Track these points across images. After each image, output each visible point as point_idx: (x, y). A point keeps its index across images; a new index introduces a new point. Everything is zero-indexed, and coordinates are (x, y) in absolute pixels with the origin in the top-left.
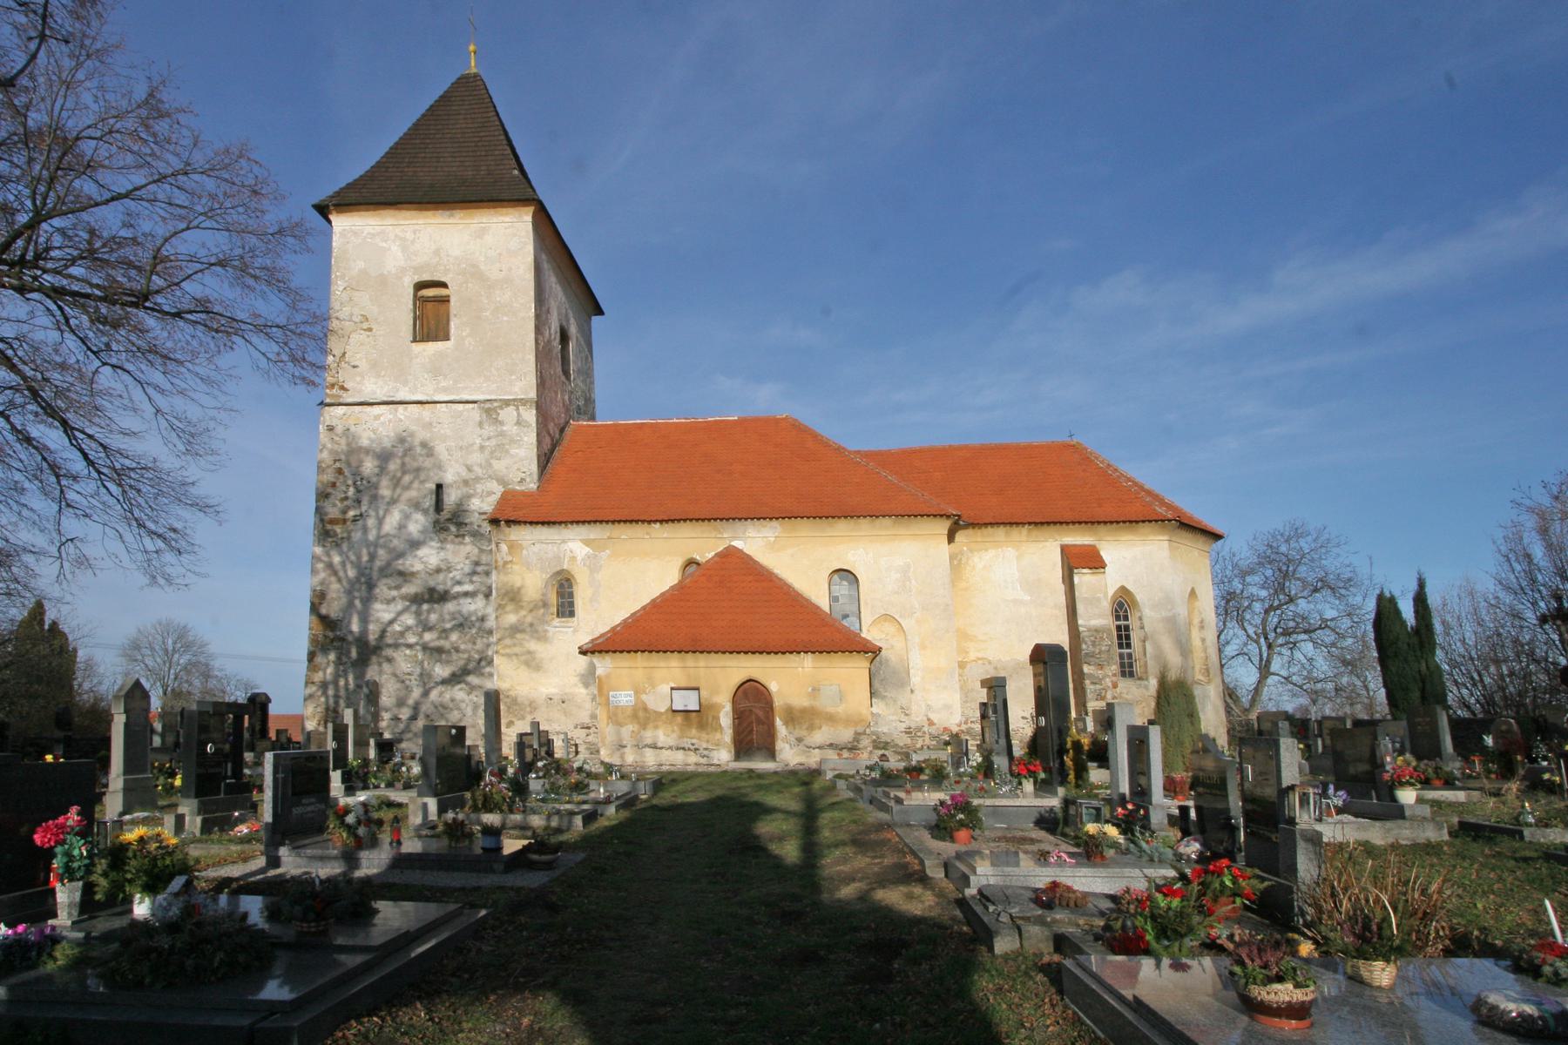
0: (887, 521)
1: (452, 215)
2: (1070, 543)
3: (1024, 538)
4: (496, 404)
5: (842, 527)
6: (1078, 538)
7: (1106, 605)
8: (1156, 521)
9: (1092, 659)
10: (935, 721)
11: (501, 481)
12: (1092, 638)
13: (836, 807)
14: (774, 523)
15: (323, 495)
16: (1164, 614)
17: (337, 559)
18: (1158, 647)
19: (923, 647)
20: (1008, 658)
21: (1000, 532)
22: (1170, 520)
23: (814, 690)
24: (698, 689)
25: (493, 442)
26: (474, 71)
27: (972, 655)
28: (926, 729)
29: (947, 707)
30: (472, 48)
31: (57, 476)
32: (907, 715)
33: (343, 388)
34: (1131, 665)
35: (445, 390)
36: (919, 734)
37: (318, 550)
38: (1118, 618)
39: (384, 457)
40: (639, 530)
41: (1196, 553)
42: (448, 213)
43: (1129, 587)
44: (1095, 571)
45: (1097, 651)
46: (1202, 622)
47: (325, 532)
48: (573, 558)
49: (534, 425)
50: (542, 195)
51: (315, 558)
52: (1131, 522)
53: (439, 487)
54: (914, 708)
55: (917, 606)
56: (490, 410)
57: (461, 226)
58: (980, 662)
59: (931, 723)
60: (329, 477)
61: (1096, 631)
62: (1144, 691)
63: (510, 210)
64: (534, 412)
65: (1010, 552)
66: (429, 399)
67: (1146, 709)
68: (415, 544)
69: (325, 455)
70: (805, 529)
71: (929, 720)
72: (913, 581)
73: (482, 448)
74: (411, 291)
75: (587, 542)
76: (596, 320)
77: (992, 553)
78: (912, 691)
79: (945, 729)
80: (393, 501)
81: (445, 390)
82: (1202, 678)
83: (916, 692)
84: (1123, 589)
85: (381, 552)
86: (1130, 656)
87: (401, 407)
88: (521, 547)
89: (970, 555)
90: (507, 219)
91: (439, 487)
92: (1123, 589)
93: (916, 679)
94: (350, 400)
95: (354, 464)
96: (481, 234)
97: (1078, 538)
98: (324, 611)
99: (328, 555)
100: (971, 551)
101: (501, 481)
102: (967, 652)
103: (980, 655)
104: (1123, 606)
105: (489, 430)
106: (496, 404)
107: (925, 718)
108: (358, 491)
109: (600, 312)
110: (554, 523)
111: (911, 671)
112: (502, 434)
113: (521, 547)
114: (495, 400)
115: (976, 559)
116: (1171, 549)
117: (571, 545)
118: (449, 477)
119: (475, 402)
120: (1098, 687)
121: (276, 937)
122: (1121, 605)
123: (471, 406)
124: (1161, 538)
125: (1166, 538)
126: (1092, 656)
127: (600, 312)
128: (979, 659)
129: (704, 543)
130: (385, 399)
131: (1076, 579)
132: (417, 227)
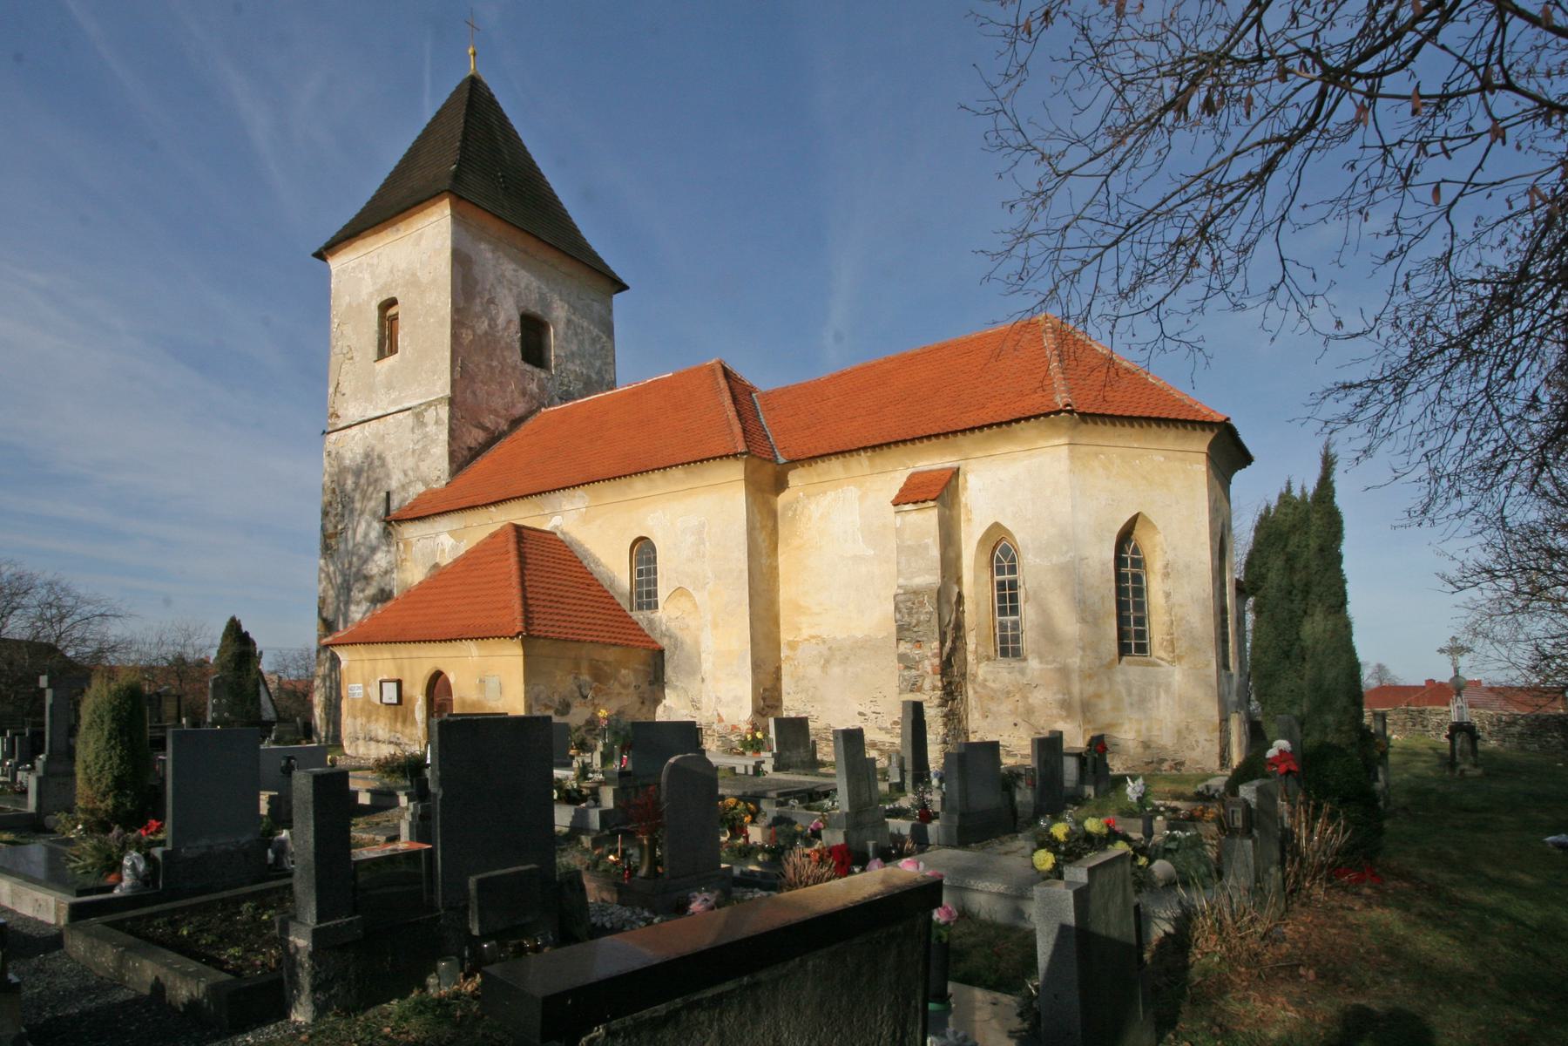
0: (677, 473)
1: (398, 230)
2: (926, 468)
3: (868, 471)
4: (423, 407)
5: (639, 485)
6: (932, 460)
8: (1047, 415)
9: (907, 633)
10: (724, 718)
11: (425, 483)
12: (909, 604)
14: (579, 492)
15: (325, 514)
16: (1055, 559)
17: (332, 569)
18: (1044, 611)
19: (715, 626)
20: (845, 636)
21: (835, 466)
22: (1057, 413)
23: (480, 681)
24: (381, 682)
25: (421, 444)
27: (806, 633)
28: (715, 726)
29: (737, 699)
32: (698, 709)
33: (338, 417)
34: (1016, 639)
35: (394, 402)
36: (709, 732)
37: (322, 562)
39: (358, 473)
41: (1158, 458)
42: (394, 229)
43: (1005, 524)
44: (921, 505)
45: (914, 622)
46: (1166, 566)
47: (327, 549)
49: (447, 421)
51: (321, 569)
52: (999, 424)
53: (388, 494)
54: (705, 700)
55: (710, 575)
56: (418, 413)
57: (406, 238)
58: (814, 641)
59: (721, 720)
60: (327, 498)
61: (915, 593)
62: (1019, 677)
63: (434, 209)
64: (447, 408)
65: (852, 492)
66: (385, 413)
67: (1020, 704)
68: (374, 550)
69: (326, 478)
70: (609, 492)
71: (719, 715)
72: (708, 544)
73: (414, 451)
74: (376, 313)
76: (618, 298)
77: (831, 495)
78: (703, 680)
79: (734, 727)
80: (362, 513)
81: (394, 402)
82: (1163, 654)
83: (707, 681)
85: (355, 559)
86: (1016, 625)
87: (366, 425)
89: (806, 502)
90: (434, 219)
91: (388, 494)
93: (707, 666)
94: (341, 426)
95: (342, 483)
96: (417, 242)
97: (948, 459)
98: (325, 615)
99: (327, 566)
100: (808, 497)
101: (425, 483)
102: (799, 629)
103: (813, 632)
105: (418, 434)
106: (423, 407)
107: (715, 713)
108: (344, 507)
109: (621, 287)
110: (428, 517)
111: (703, 656)
112: (425, 436)
114: (421, 404)
115: (813, 507)
116: (1072, 457)
118: (394, 484)
119: (409, 409)
120: (914, 672)
123: (407, 413)
124: (1056, 442)
125: (1064, 440)
126: (908, 630)
127: (621, 287)
128: (813, 637)
130: (360, 420)
132: (379, 251)
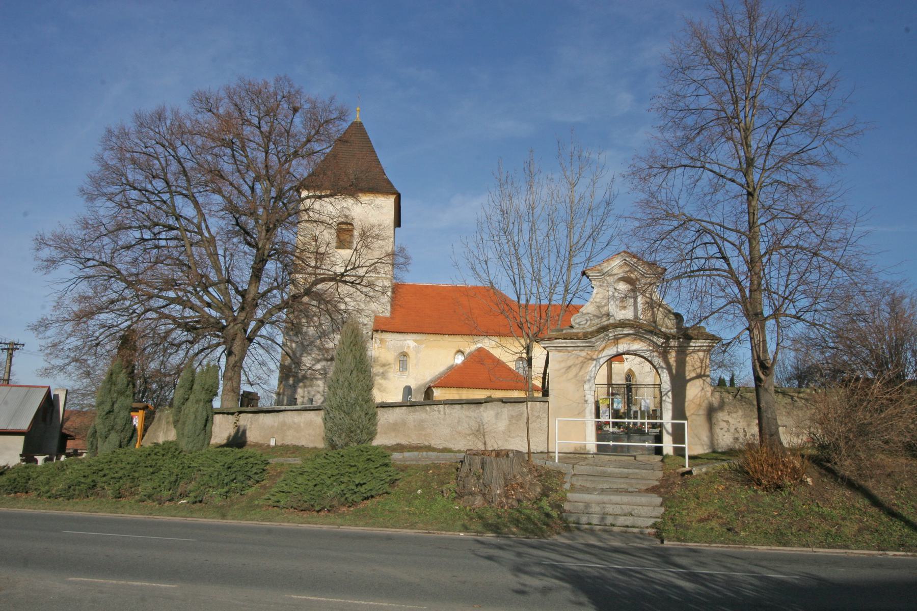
7: (623, 376)
13: (9, 358)
26: (359, 120)
30: (358, 109)
31: (731, 271)
38: (627, 381)
40: (439, 337)
48: (409, 347)
50: (398, 187)
75: (415, 341)
84: (630, 370)
88: (386, 341)
92: (630, 370)
104: (630, 375)
113: (386, 341)
117: (408, 341)
121: (51, 419)
122: (629, 376)
129: (470, 345)
131: (613, 365)
